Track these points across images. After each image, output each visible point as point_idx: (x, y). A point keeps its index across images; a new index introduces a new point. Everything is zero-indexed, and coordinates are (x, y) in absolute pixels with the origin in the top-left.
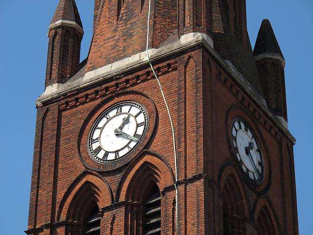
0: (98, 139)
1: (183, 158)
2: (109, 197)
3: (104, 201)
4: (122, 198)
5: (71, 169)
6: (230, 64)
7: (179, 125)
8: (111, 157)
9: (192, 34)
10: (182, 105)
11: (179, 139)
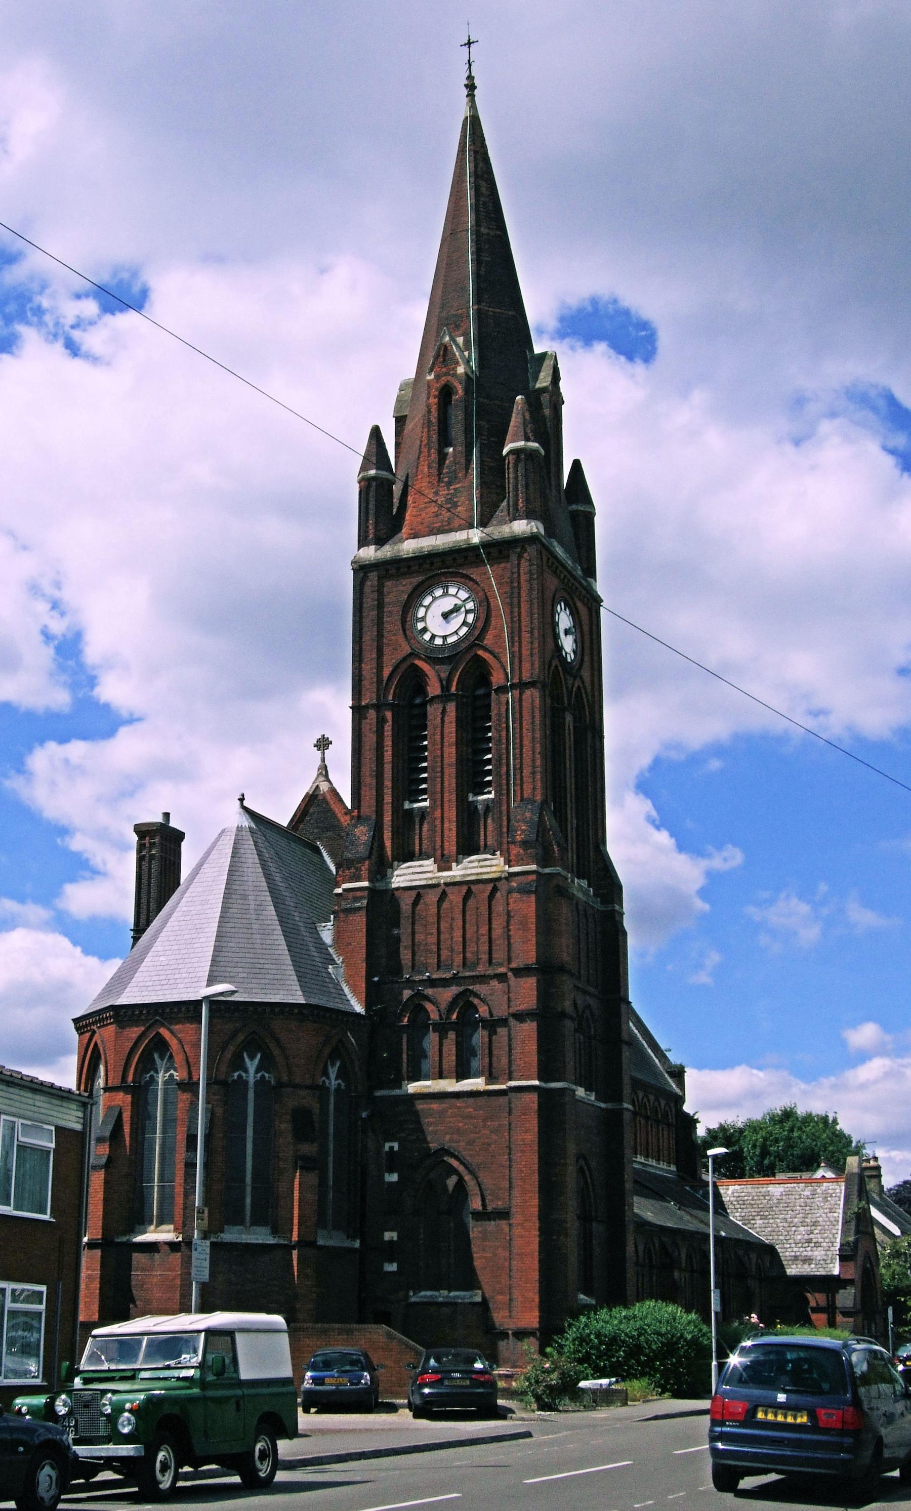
0: (423, 619)
1: (517, 658)
2: (438, 685)
3: (434, 689)
4: (453, 689)
5: (397, 650)
6: (555, 544)
7: (512, 622)
8: (438, 641)
9: (525, 521)
10: (516, 600)
11: (512, 638)
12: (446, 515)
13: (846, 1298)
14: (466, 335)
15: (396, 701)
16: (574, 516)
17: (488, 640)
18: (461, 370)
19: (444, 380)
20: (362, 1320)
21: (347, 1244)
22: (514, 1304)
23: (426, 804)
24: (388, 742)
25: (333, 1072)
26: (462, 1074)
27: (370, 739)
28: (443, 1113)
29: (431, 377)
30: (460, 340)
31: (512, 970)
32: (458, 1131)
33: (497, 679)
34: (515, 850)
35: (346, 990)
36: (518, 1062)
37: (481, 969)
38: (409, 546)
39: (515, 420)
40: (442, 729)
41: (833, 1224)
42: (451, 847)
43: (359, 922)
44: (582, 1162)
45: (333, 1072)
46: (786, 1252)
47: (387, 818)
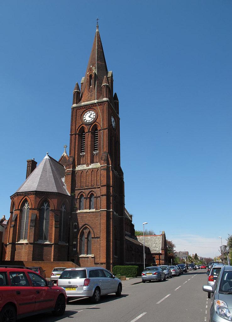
1: (103, 124)
3: (86, 130)
8: (88, 121)
12: (90, 98)
13: (162, 257)
14: (95, 67)
15: (80, 134)
16: (115, 103)
17: (97, 121)
18: (94, 72)
19: (90, 74)
20: (68, 261)
21: (65, 244)
22: (101, 257)
23: (85, 154)
24: (77, 141)
25: (63, 208)
26: (90, 209)
27: (73, 141)
28: (86, 217)
29: (88, 73)
30: (94, 68)
31: (101, 186)
32: (89, 220)
33: (99, 129)
34: (102, 161)
35: (67, 191)
36: (102, 205)
37: (95, 186)
38: (83, 104)
39: (104, 80)
40: (88, 138)
41: (160, 243)
42: (89, 162)
43: (70, 177)
44: (115, 227)
45: (63, 208)
46: (151, 249)
47: (76, 156)
